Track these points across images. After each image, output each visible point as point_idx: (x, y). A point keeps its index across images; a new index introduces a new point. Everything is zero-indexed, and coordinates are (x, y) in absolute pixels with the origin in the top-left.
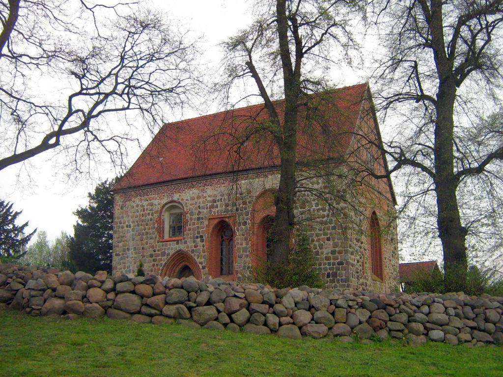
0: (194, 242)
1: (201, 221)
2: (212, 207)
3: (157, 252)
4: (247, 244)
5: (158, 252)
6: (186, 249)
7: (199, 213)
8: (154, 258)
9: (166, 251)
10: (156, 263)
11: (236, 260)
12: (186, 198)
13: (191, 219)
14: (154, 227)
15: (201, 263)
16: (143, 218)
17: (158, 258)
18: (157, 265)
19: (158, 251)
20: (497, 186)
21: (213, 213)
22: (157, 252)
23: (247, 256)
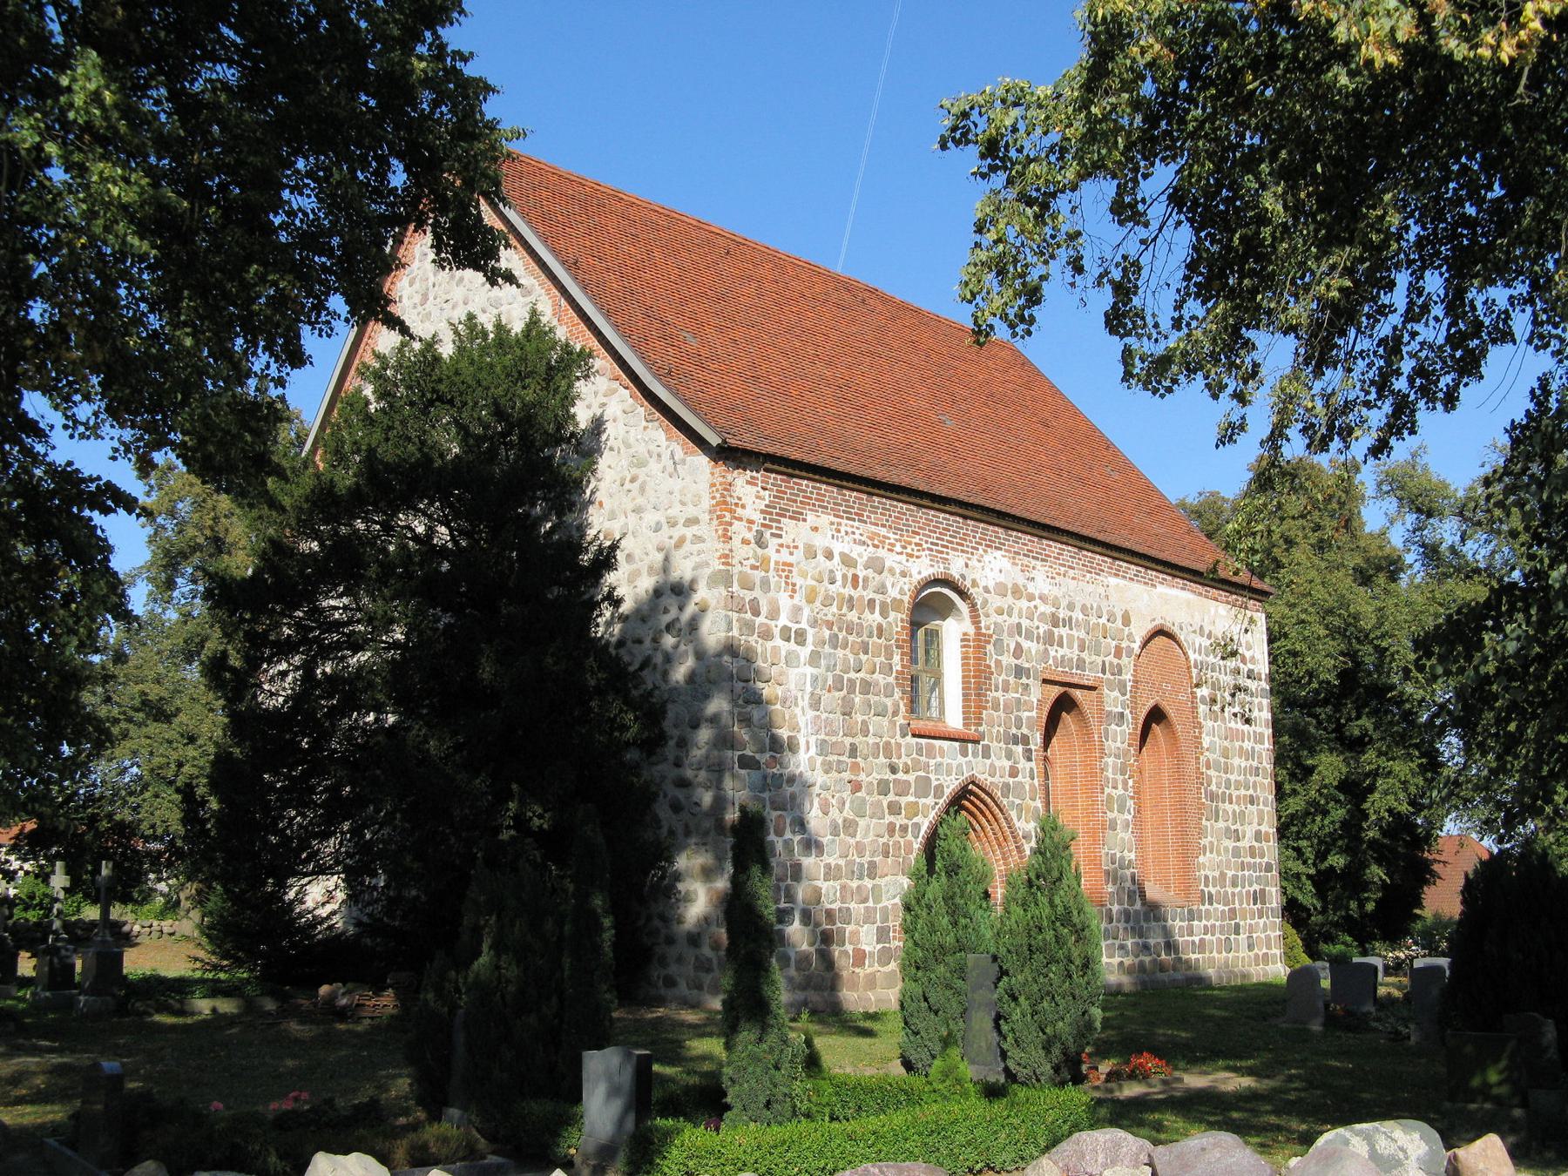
2: (1049, 639)
9: (932, 777)
18: (904, 829)
21: (1051, 662)
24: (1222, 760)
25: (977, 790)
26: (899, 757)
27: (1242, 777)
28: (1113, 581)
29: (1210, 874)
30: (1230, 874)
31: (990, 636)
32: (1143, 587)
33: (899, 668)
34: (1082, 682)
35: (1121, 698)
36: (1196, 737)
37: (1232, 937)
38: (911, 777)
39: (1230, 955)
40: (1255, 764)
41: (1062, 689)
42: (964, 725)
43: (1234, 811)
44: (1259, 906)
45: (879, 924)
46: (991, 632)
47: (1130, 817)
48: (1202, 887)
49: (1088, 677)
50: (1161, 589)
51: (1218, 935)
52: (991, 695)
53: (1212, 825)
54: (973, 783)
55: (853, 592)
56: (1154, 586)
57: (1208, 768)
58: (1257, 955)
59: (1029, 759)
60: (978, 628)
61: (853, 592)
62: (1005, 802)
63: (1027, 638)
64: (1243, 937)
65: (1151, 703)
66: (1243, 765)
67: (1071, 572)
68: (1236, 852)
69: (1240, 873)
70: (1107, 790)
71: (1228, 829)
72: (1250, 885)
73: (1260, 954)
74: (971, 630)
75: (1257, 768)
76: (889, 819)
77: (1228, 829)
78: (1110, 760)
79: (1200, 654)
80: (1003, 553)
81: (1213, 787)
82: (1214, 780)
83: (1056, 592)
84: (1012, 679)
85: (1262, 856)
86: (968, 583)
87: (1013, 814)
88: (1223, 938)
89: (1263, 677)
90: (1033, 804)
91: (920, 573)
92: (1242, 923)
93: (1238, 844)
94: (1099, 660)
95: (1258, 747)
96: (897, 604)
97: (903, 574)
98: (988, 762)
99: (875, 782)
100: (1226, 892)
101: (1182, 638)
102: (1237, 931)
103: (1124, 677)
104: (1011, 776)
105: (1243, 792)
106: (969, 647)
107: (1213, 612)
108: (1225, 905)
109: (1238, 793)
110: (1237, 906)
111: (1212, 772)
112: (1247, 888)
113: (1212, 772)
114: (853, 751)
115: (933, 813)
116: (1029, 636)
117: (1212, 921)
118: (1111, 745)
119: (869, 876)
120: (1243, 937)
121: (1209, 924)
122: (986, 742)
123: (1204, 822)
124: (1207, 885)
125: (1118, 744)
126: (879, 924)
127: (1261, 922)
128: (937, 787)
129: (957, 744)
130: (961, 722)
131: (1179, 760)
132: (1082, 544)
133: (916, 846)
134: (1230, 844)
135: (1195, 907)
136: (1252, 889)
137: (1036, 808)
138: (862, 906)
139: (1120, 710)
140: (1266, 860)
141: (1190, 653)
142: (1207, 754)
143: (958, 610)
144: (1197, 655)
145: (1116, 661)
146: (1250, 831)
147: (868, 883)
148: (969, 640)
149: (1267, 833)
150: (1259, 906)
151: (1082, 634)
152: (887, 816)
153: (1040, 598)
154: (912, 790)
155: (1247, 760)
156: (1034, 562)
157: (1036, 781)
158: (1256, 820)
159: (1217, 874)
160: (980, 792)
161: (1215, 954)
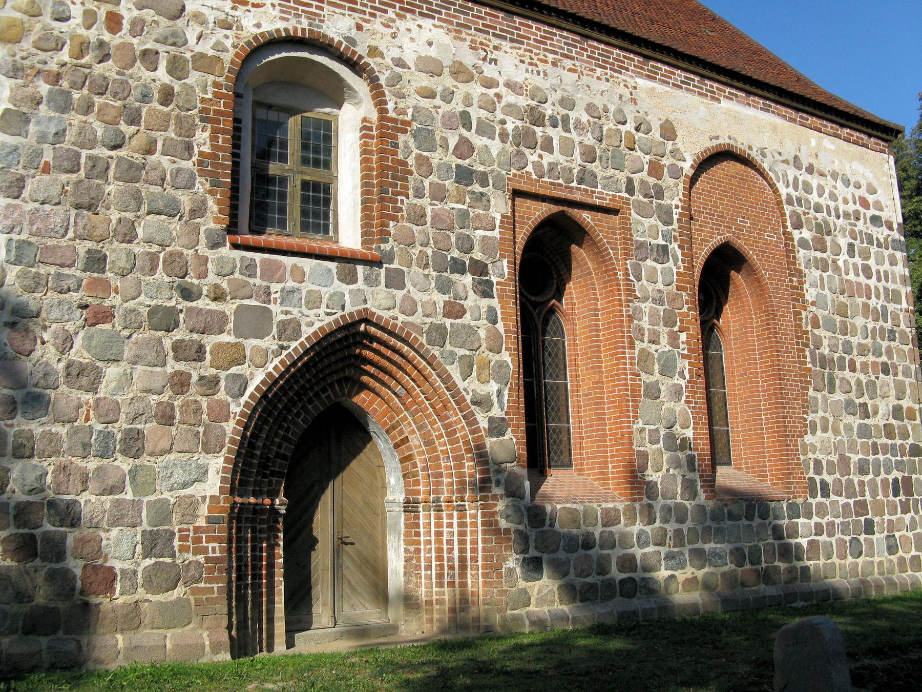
0: (444, 287)
1: (477, 188)
2: (525, 139)
3: (204, 303)
4: (674, 340)
5: (213, 306)
6: (402, 318)
7: (465, 148)
8: (179, 334)
9: (275, 308)
10: (195, 372)
11: (635, 407)
12: (395, 53)
13: (424, 162)
14: (189, 148)
15: (482, 402)
16: (98, 69)
17: (210, 341)
18: (210, 384)
19: (218, 297)
20: (347, 567)
21: (529, 168)
22: (204, 303)
23: (677, 393)
24: (838, 319)
25: (379, 333)
26: (203, 275)
27: (869, 341)
28: (642, 82)
29: (824, 458)
30: (855, 458)
31: (409, 124)
32: (698, 99)
33: (207, 149)
34: (589, 200)
35: (662, 227)
36: (796, 288)
37: (862, 537)
38: (229, 308)
39: (860, 560)
40: (888, 325)
41: (555, 209)
42: (363, 243)
43: (859, 382)
44: (902, 498)
45: (145, 526)
46: (409, 118)
47: (683, 383)
48: (811, 474)
49: (602, 195)
50: (725, 104)
51: (839, 535)
52: (406, 203)
53: (824, 397)
54: (367, 321)
55: (107, 37)
56: (718, 100)
57: (816, 325)
58: (902, 560)
59: (487, 294)
60: (383, 111)
61: (107, 37)
62: (436, 351)
63: (480, 132)
64: (878, 537)
65: (716, 240)
66: (870, 326)
67: (568, 63)
68: (864, 432)
69: (871, 458)
70: (639, 345)
71: (849, 403)
72: (888, 472)
73: (907, 556)
74: (374, 116)
75: (892, 332)
76: (173, 366)
77: (849, 403)
78: (646, 307)
79: (796, 189)
80: (436, 22)
81: (825, 351)
82: (825, 342)
83: (538, 81)
84: (450, 184)
85: (905, 436)
86: (361, 50)
87: (454, 371)
88: (847, 538)
89: (895, 226)
90: (494, 358)
91: (895, 297)
92: (876, 519)
93: (866, 421)
94: (622, 176)
95: (891, 307)
96: (203, 63)
97: (226, 25)
98: (400, 294)
99: (144, 311)
100: (850, 482)
101: (766, 166)
102: (869, 528)
103: (666, 202)
104: (447, 315)
105: (871, 358)
106: (372, 137)
107: (813, 143)
108: (848, 497)
109: (863, 359)
110: (868, 497)
111: (821, 332)
112: (883, 475)
113: (821, 332)
114: (96, 261)
115: (276, 361)
116: (485, 129)
117: (828, 518)
118: (643, 286)
119: (125, 452)
120: (878, 537)
121: (824, 522)
122: (395, 265)
123: (811, 392)
124: (818, 471)
125: (660, 286)
126: (145, 526)
127: (907, 517)
128: (283, 326)
129: (333, 266)
130: (360, 240)
131: (770, 315)
132: (587, 32)
133: (236, 408)
134: (855, 421)
135: (800, 501)
136: (891, 478)
137: (501, 365)
138: (108, 499)
139: (661, 241)
140: (911, 441)
141: (780, 186)
142: (813, 309)
143: (350, 88)
144: (791, 190)
145: (652, 181)
146: (884, 407)
147: (124, 464)
148: (370, 129)
149: (910, 410)
150: (902, 498)
151: (589, 140)
152: (171, 361)
153: (508, 85)
154: (231, 325)
155: (876, 320)
156: (496, 42)
157: (500, 326)
158: (893, 393)
159: (835, 458)
160: (386, 337)
161: (835, 559)
